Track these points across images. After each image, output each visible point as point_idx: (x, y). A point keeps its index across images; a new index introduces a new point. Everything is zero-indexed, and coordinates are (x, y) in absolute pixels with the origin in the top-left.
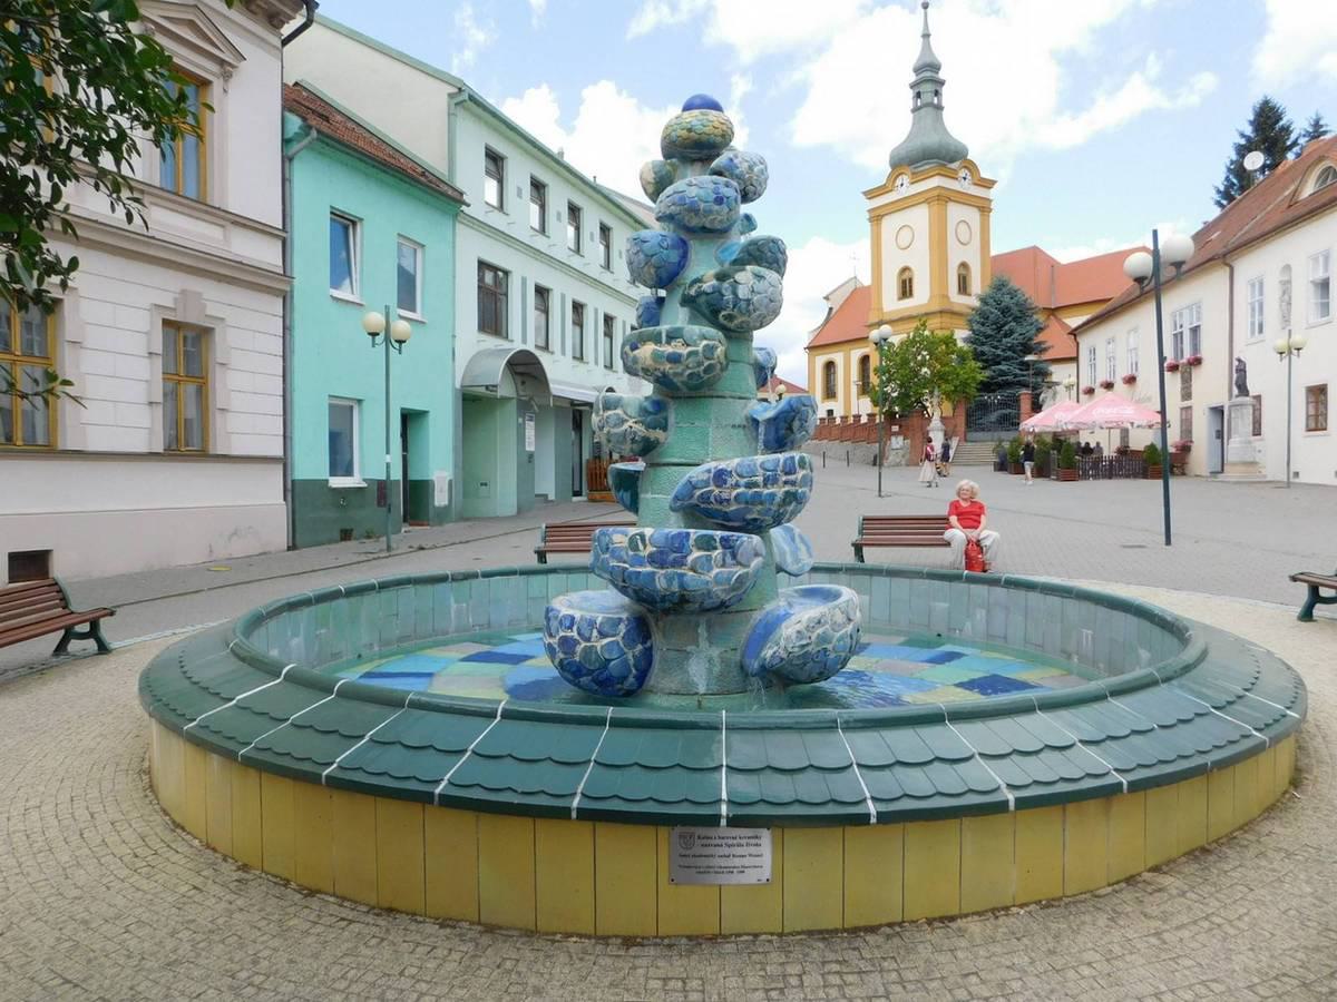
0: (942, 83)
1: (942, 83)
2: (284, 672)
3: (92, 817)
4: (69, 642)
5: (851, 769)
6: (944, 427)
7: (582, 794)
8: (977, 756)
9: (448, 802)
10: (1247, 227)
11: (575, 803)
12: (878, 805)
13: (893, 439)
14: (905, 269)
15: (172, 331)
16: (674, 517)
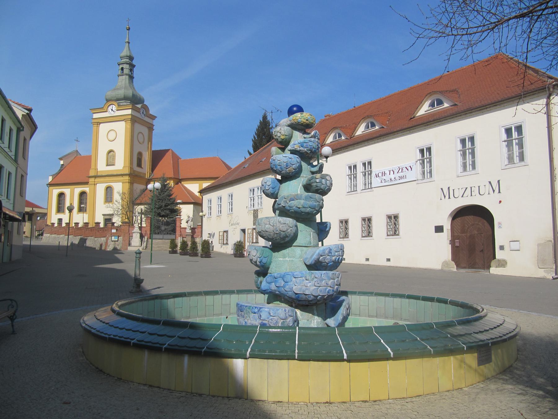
0: (134, 66)
1: (134, 66)
6: (140, 232)
13: (143, 226)
14: (111, 151)
16: (204, 239)
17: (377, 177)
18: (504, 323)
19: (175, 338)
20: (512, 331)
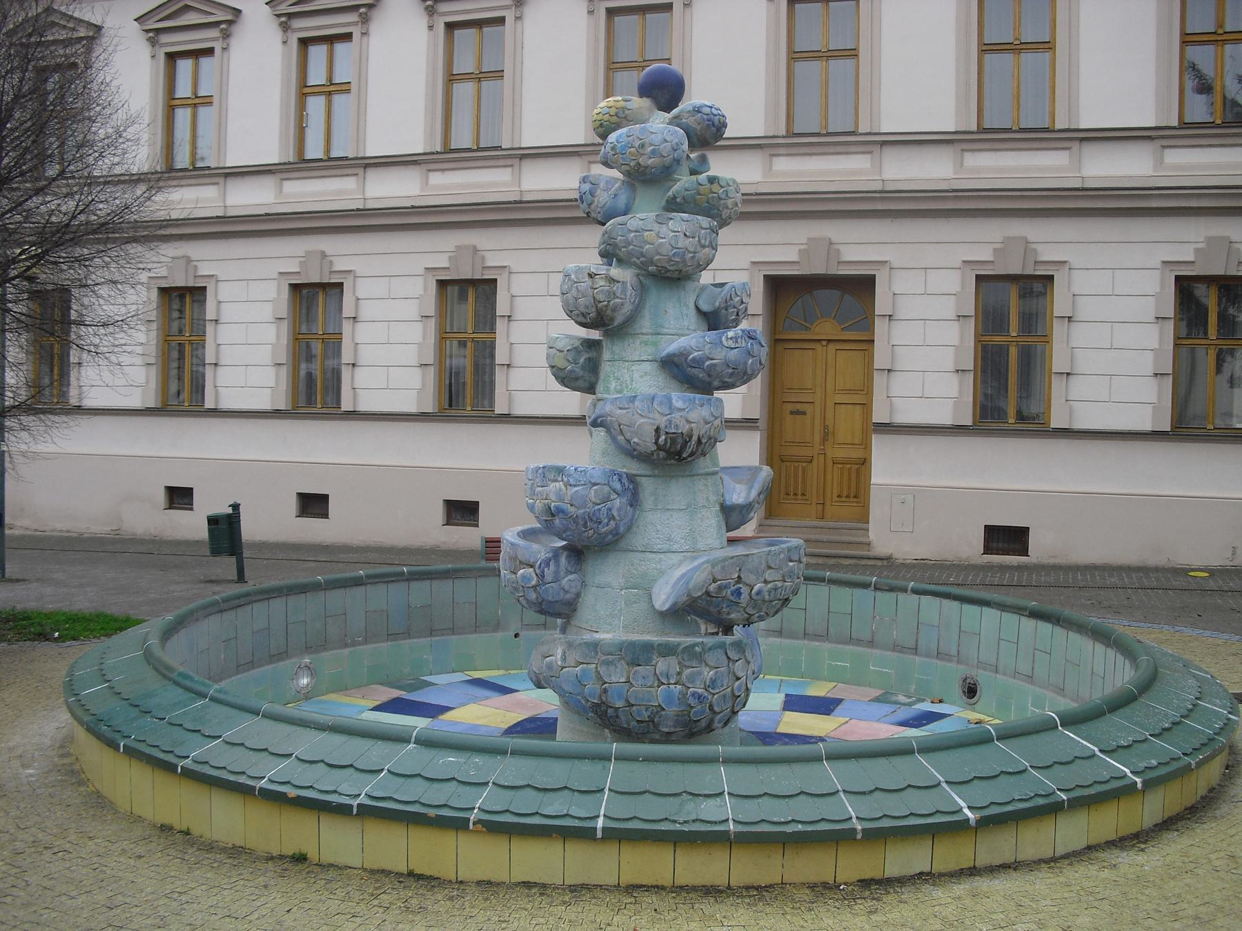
2: (414, 734)
5: (722, 796)
7: (605, 816)
9: (188, 774)
10: (117, 235)
11: (600, 823)
12: (737, 825)
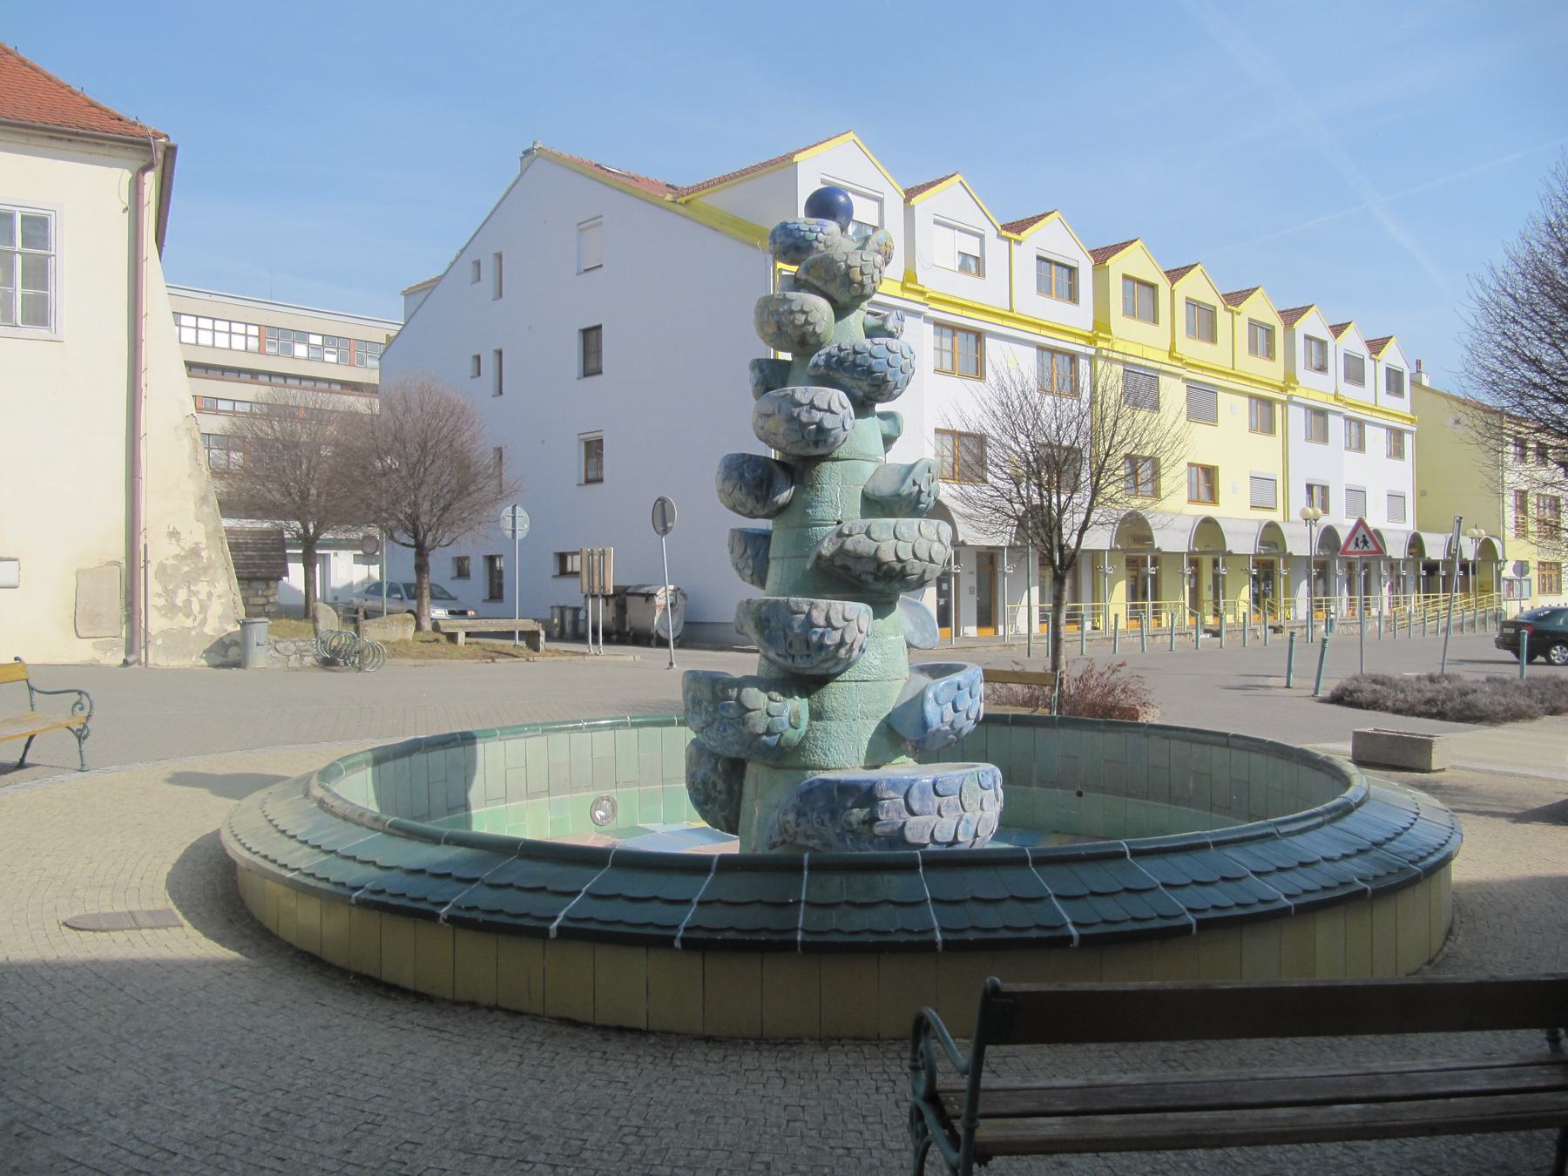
3: (825, 1118)
4: (847, 550)
8: (1161, 888)
15: (1308, 341)
17: (601, 223)
18: (1416, 823)
19: (579, 897)
20: (1437, 850)
